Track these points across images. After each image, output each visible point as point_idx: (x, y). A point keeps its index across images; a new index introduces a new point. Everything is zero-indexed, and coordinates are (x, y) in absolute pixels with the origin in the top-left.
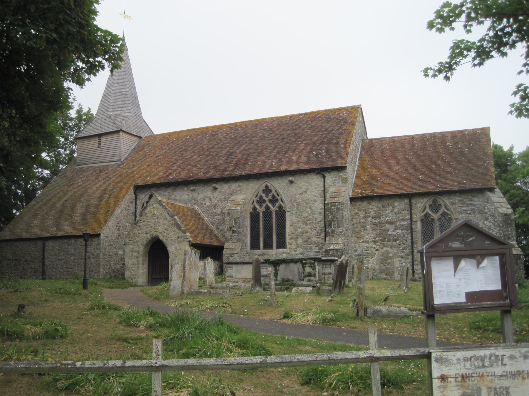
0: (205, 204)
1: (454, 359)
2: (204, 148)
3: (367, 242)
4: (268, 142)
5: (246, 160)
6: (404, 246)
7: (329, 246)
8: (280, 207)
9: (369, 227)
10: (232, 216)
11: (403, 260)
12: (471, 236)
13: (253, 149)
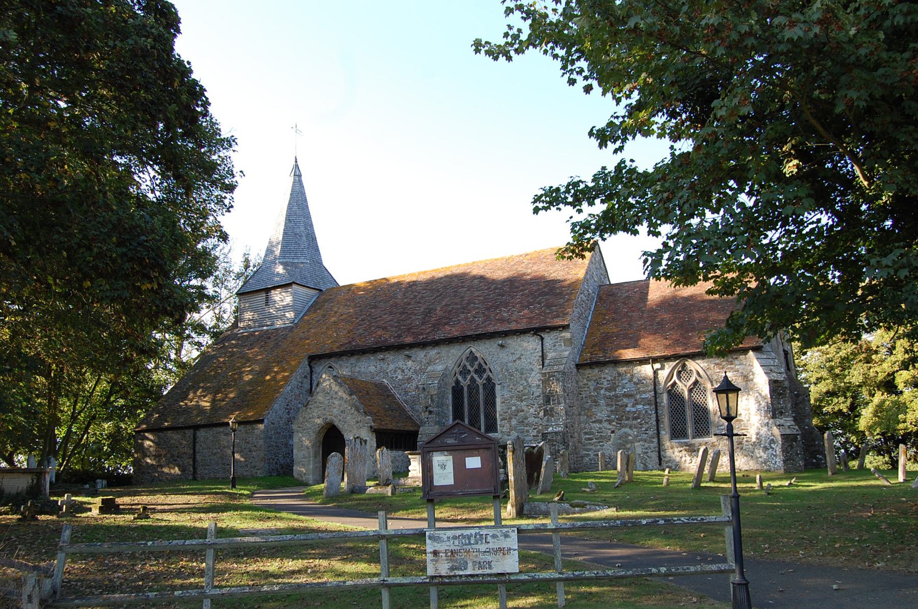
0: (397, 377)
1: (445, 538)
2: (397, 304)
3: (600, 422)
4: (477, 293)
5: (447, 318)
6: (647, 426)
7: (547, 429)
8: (489, 379)
9: (602, 402)
10: (428, 392)
11: (647, 445)
12: (464, 433)
13: (457, 304)
